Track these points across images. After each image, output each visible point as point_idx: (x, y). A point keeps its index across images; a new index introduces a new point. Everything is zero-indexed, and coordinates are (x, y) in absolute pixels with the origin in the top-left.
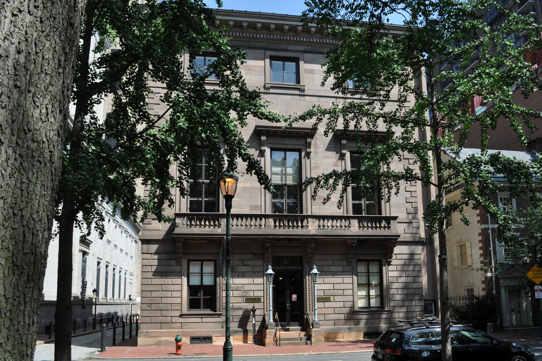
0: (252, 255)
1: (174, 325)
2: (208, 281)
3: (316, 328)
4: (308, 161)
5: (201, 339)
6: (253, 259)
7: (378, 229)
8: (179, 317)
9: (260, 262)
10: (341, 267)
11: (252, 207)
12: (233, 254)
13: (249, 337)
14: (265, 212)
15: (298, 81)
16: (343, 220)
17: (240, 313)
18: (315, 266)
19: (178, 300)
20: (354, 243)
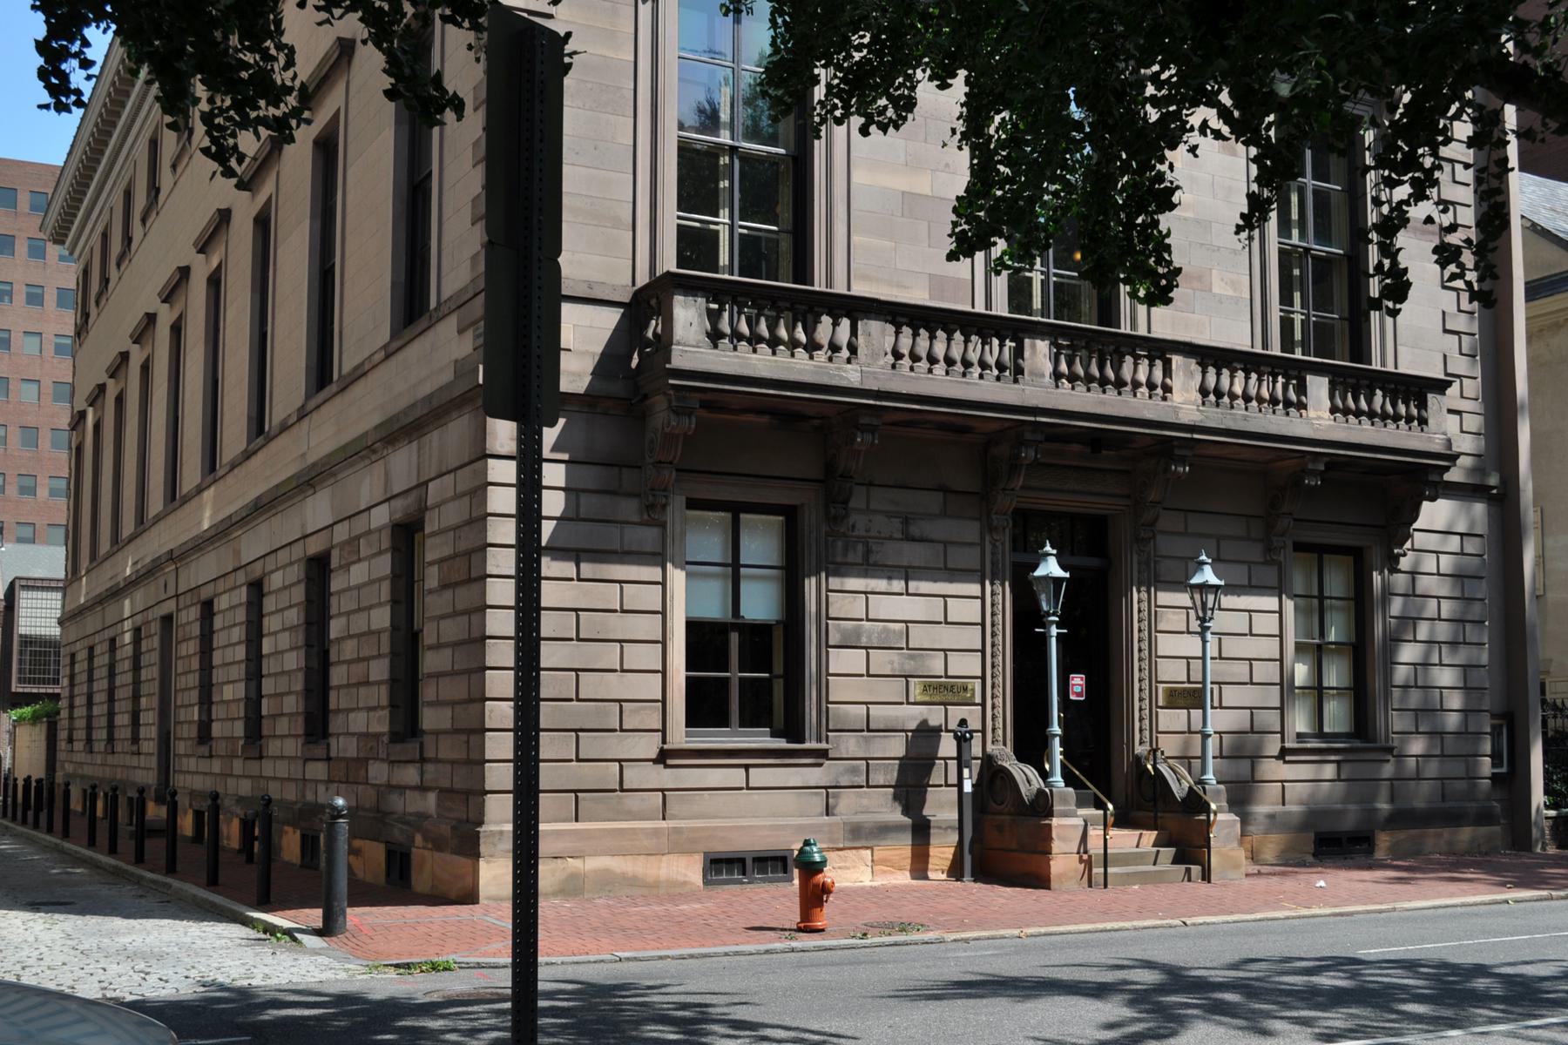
0: (939, 496)
1: (633, 801)
2: (760, 604)
3: (674, 817)
5: (749, 863)
6: (944, 514)
7: (821, 356)
8: (655, 761)
12: (871, 484)
13: (933, 851)
14: (988, 305)
16: (958, 336)
17: (896, 747)
20: (1313, 473)
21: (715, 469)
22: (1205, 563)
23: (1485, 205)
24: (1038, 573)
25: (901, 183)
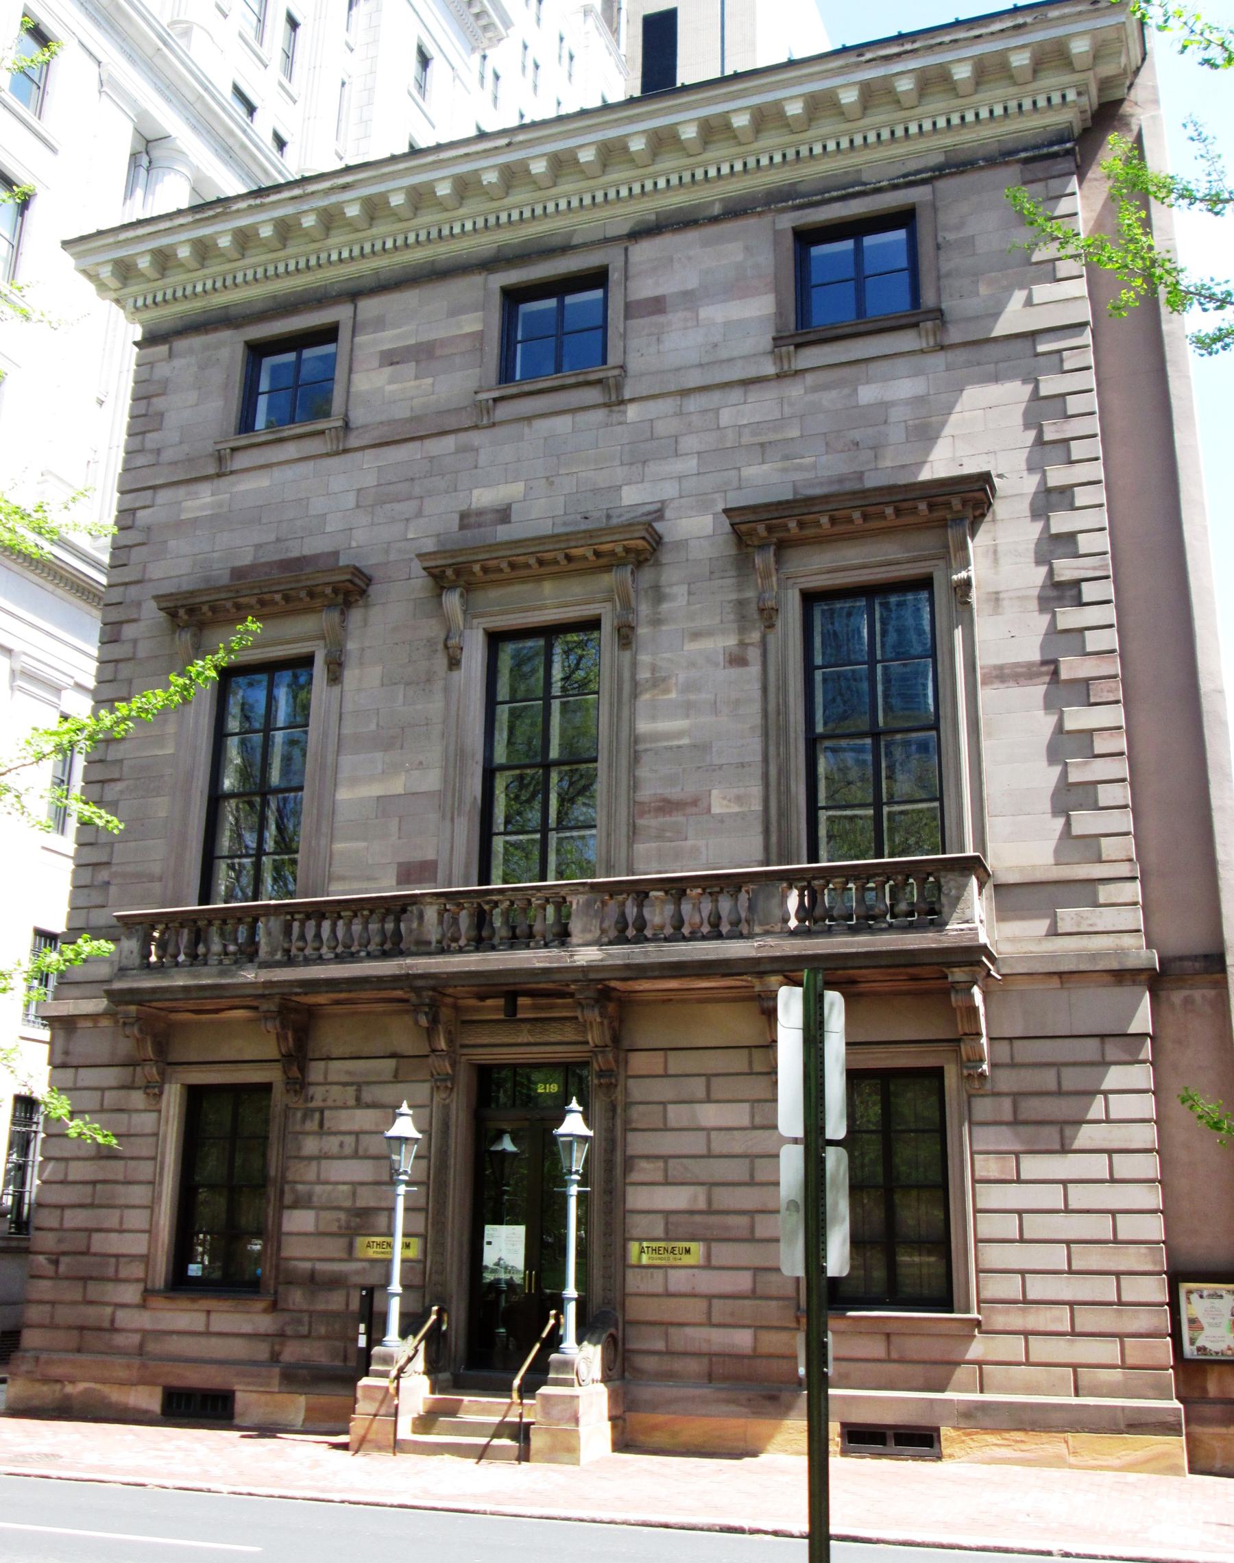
0: (392, 1063)
11: (408, 874)
19: (138, 1245)
25: (376, 790)
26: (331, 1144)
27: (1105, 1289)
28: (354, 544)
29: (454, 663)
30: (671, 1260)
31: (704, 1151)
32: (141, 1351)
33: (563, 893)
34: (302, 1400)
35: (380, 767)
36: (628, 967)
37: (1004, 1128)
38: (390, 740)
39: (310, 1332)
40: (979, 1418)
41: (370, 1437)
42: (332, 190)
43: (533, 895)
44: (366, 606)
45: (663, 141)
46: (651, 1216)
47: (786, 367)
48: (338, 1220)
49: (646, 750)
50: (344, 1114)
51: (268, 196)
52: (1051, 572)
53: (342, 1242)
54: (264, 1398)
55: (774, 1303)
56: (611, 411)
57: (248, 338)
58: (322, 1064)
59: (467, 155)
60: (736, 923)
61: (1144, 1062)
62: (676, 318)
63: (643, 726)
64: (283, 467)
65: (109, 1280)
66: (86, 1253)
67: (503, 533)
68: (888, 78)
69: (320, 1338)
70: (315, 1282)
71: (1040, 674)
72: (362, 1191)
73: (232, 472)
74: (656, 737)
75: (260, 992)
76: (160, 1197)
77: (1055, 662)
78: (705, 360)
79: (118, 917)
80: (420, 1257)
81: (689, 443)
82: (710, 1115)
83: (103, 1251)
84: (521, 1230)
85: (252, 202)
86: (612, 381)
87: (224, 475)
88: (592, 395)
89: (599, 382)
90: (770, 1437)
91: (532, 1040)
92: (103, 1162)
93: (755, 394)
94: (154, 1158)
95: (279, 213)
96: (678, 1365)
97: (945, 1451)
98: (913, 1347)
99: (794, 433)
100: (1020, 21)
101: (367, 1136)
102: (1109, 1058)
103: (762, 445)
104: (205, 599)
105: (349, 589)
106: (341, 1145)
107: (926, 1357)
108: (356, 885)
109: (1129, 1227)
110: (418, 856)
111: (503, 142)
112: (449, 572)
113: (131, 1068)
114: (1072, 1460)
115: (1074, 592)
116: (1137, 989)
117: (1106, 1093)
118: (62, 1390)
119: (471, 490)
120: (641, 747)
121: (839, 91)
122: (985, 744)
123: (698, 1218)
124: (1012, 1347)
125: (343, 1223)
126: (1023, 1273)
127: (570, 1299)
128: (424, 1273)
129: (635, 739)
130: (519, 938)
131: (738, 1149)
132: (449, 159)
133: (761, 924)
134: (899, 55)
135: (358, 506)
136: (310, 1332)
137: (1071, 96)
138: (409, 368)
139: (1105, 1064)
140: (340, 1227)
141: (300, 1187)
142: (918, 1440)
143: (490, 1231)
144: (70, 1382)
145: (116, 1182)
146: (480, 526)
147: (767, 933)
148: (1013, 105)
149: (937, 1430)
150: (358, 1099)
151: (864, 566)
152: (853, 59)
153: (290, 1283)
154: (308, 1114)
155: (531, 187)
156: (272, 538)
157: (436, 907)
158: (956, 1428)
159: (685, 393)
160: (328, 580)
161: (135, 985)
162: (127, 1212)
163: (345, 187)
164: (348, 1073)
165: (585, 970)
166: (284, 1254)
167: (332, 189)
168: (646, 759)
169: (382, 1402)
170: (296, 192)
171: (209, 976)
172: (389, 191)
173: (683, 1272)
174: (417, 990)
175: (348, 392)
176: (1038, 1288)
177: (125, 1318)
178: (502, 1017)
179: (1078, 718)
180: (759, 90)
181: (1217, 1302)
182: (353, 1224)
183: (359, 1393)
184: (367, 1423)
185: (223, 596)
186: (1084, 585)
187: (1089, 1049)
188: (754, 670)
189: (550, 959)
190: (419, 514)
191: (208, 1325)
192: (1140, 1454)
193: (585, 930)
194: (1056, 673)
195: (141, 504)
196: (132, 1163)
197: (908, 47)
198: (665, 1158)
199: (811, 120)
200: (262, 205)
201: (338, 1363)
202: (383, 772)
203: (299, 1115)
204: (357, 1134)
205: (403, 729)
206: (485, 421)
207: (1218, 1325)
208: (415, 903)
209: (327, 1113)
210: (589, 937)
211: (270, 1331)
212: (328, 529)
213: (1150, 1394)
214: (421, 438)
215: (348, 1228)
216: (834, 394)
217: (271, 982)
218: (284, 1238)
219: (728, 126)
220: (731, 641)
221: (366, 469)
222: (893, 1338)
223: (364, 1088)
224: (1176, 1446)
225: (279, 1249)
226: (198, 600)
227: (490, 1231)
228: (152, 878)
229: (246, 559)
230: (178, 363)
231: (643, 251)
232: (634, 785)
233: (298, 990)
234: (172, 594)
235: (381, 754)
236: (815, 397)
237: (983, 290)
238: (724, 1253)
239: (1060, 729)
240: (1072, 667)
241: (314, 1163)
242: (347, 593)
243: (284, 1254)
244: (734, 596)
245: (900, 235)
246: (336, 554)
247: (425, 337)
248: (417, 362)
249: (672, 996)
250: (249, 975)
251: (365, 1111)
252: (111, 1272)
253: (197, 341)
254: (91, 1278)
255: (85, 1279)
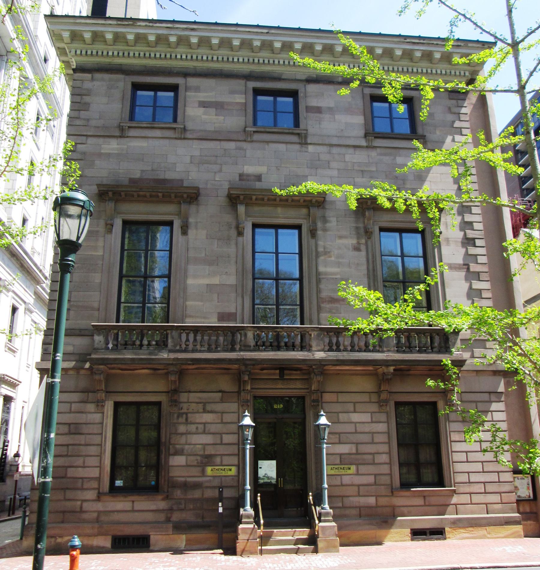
0: (220, 394)
3: (325, 521)
4: (312, 242)
6: (222, 401)
9: (234, 406)
10: (69, 475)
11: (222, 317)
15: (297, 124)
18: (322, 413)
19: (95, 473)
21: (129, 391)
22: (323, 415)
23: (295, 313)
24: (254, 425)
25: (206, 281)
26: (193, 428)
27: (494, 477)
28: (190, 178)
29: (240, 233)
30: (343, 472)
31: (354, 431)
32: (97, 520)
33: (308, 330)
34: (184, 537)
35: (207, 272)
36: (338, 360)
37: (460, 423)
38: (213, 261)
39: (185, 507)
40: (457, 524)
41: (246, 549)
42: (186, 29)
43: (295, 330)
44: (198, 205)
45: (97, 37)
46: (335, 456)
47: (370, 144)
48: (197, 460)
49: (323, 278)
50: (197, 415)
51: (156, 23)
52: (465, 234)
53: (200, 469)
54: (164, 537)
55: (383, 487)
56: (302, 146)
57: (134, 81)
58: (186, 394)
59: (249, 32)
60: (374, 346)
61: (502, 401)
62: (326, 116)
63: (321, 269)
64: (154, 139)
65: (77, 489)
66: (65, 477)
67: (258, 185)
68: (412, 50)
69: (190, 510)
70: (186, 486)
71: (463, 268)
72: (207, 447)
73: (128, 137)
74: (326, 274)
75: (171, 362)
76: (105, 451)
77: (468, 265)
78: (338, 135)
79: (92, 325)
80: (236, 474)
81: (334, 165)
82: (355, 417)
83: (74, 476)
84: (274, 462)
85: (148, 24)
86: (303, 135)
87: (124, 137)
88: (295, 139)
89: (298, 134)
90: (385, 536)
91: (283, 387)
92: (72, 436)
93: (358, 152)
94: (102, 434)
95: (160, 32)
96: (348, 512)
97: (447, 536)
98: (433, 500)
99: (374, 169)
100: (459, 44)
101: (209, 425)
102: (492, 400)
103: (362, 171)
104: (124, 189)
105: (191, 196)
106: (197, 428)
107: (438, 503)
108: (198, 320)
109: (463, 457)
110: (227, 310)
111: (265, 31)
112: (242, 197)
113: (87, 393)
114: (489, 536)
115: (472, 242)
116: (500, 377)
117: (492, 411)
118: (55, 541)
119: (243, 166)
120: (321, 277)
121: (396, 50)
122: (447, 290)
123: (353, 456)
124: (465, 499)
125: (199, 461)
126: (468, 473)
127: (326, 488)
128: (239, 481)
129: (318, 273)
130: (291, 347)
131: (367, 430)
132: (241, 31)
133: (386, 347)
134: (418, 43)
135: (191, 163)
136: (185, 507)
137: (467, 74)
138: (212, 111)
139: (491, 402)
140: (198, 463)
141: (178, 446)
142: (437, 533)
143: (261, 463)
144: (60, 537)
145: (80, 445)
146: (248, 181)
147: (388, 351)
148: (448, 71)
149: (444, 529)
150: (204, 409)
151: (402, 222)
152: (403, 40)
153: (175, 487)
154: (180, 415)
155: (125, 44)
156: (149, 168)
157: (252, 332)
158: (450, 528)
159: (331, 145)
160: (186, 191)
161: (106, 356)
162: (87, 458)
163: (193, 30)
164: (200, 398)
165: (320, 361)
166: (171, 475)
167: (186, 29)
168: (323, 281)
169: (251, 534)
170: (169, 25)
171: (144, 354)
172: (212, 37)
173: (348, 476)
174: (246, 365)
175: (184, 115)
176: (474, 478)
177: (86, 506)
178: (278, 377)
179: (477, 285)
180: (327, 38)
181: (523, 481)
182: (204, 462)
183: (240, 531)
184: (245, 544)
185: (134, 190)
186: (476, 240)
187: (486, 397)
188: (363, 253)
189: (334, 356)
190: (220, 171)
191: (133, 507)
192: (509, 532)
193: (317, 345)
194: (468, 269)
195: (80, 142)
196: (88, 436)
197: (422, 41)
198: (339, 434)
199: (240, 48)
200: (152, 26)
201: (200, 520)
202: (209, 274)
203: (176, 415)
204: (204, 424)
205: (217, 257)
206: (249, 139)
207: (523, 488)
208: (243, 330)
209: (189, 415)
210: (319, 348)
211: (165, 509)
212: (177, 170)
213: (510, 512)
214: (220, 140)
215: (202, 463)
216: (387, 158)
217: (177, 359)
218: (170, 468)
219: (104, 37)
220: (354, 241)
221: (196, 148)
222: (427, 498)
223: (207, 405)
224: (519, 528)
225: (168, 473)
226: (120, 189)
227: (261, 463)
228: (93, 309)
229: (137, 175)
230: (96, 83)
231: (312, 88)
232: (319, 291)
233: (190, 362)
234: (107, 185)
235: (208, 267)
236: (382, 157)
237: (438, 132)
238: (363, 469)
239: (470, 288)
240: (474, 267)
241: (184, 436)
242: (191, 198)
243: (171, 475)
244: (354, 225)
245: (172, 94)
246: (182, 181)
247: (219, 99)
248: (216, 109)
249: (339, 372)
250: (164, 355)
251: (207, 414)
252: (79, 485)
253: (106, 76)
254: (67, 489)
255: (65, 489)
